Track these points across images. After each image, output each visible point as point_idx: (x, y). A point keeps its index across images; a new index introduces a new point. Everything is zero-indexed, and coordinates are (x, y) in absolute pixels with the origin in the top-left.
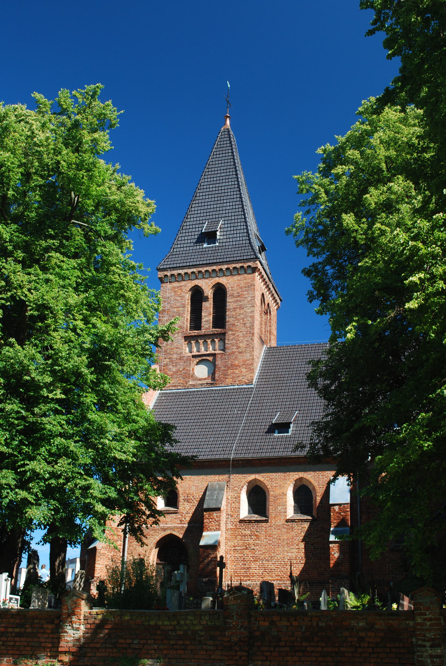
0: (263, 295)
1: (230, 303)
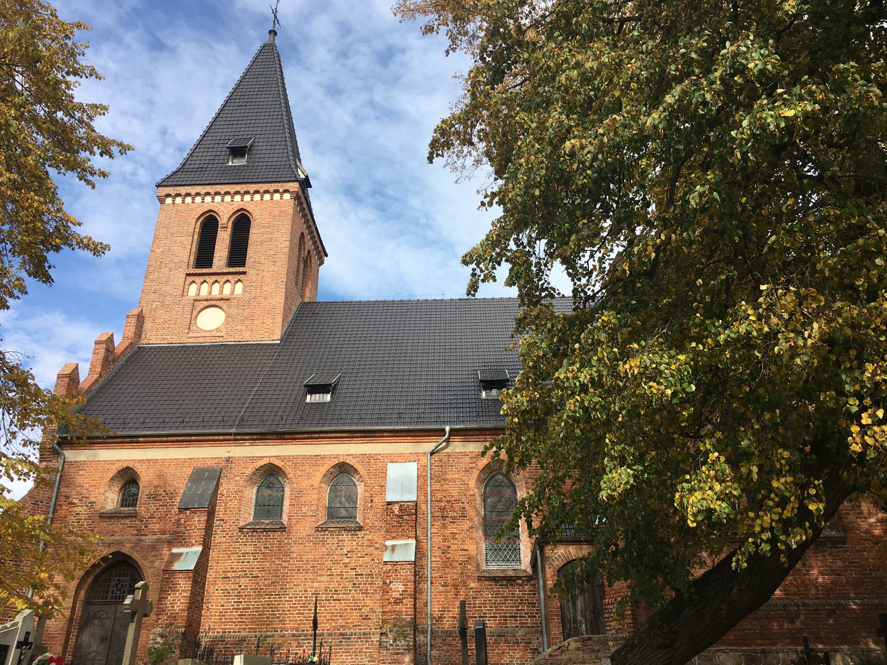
0: (302, 234)
1: (255, 234)
